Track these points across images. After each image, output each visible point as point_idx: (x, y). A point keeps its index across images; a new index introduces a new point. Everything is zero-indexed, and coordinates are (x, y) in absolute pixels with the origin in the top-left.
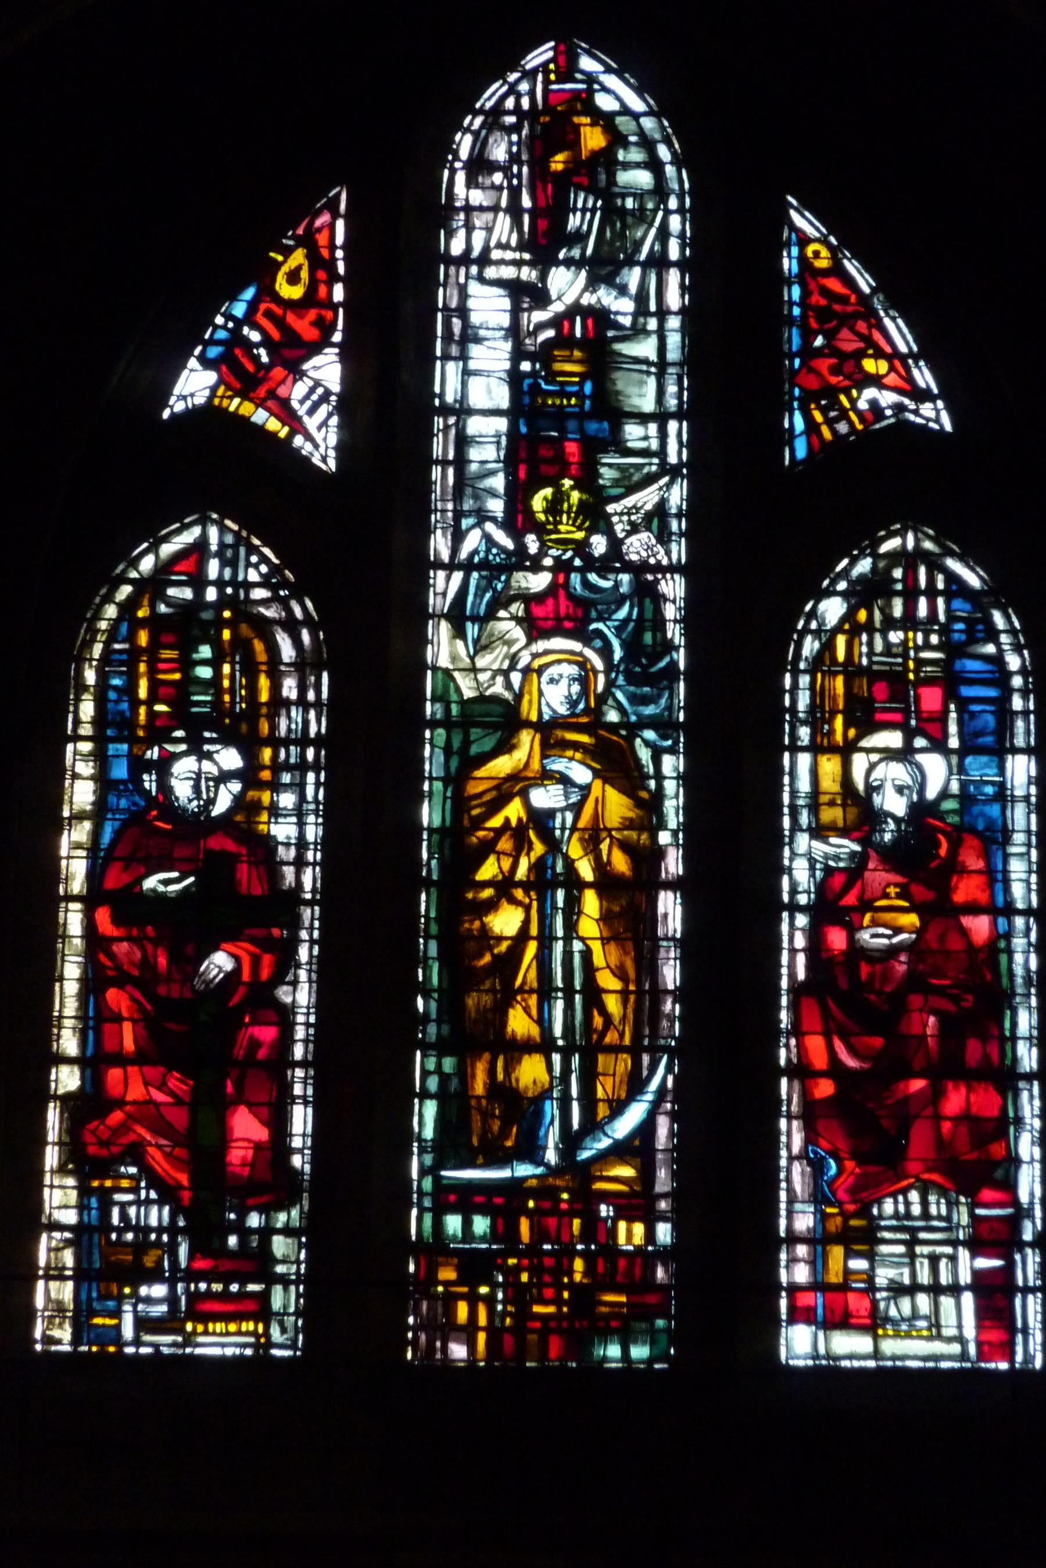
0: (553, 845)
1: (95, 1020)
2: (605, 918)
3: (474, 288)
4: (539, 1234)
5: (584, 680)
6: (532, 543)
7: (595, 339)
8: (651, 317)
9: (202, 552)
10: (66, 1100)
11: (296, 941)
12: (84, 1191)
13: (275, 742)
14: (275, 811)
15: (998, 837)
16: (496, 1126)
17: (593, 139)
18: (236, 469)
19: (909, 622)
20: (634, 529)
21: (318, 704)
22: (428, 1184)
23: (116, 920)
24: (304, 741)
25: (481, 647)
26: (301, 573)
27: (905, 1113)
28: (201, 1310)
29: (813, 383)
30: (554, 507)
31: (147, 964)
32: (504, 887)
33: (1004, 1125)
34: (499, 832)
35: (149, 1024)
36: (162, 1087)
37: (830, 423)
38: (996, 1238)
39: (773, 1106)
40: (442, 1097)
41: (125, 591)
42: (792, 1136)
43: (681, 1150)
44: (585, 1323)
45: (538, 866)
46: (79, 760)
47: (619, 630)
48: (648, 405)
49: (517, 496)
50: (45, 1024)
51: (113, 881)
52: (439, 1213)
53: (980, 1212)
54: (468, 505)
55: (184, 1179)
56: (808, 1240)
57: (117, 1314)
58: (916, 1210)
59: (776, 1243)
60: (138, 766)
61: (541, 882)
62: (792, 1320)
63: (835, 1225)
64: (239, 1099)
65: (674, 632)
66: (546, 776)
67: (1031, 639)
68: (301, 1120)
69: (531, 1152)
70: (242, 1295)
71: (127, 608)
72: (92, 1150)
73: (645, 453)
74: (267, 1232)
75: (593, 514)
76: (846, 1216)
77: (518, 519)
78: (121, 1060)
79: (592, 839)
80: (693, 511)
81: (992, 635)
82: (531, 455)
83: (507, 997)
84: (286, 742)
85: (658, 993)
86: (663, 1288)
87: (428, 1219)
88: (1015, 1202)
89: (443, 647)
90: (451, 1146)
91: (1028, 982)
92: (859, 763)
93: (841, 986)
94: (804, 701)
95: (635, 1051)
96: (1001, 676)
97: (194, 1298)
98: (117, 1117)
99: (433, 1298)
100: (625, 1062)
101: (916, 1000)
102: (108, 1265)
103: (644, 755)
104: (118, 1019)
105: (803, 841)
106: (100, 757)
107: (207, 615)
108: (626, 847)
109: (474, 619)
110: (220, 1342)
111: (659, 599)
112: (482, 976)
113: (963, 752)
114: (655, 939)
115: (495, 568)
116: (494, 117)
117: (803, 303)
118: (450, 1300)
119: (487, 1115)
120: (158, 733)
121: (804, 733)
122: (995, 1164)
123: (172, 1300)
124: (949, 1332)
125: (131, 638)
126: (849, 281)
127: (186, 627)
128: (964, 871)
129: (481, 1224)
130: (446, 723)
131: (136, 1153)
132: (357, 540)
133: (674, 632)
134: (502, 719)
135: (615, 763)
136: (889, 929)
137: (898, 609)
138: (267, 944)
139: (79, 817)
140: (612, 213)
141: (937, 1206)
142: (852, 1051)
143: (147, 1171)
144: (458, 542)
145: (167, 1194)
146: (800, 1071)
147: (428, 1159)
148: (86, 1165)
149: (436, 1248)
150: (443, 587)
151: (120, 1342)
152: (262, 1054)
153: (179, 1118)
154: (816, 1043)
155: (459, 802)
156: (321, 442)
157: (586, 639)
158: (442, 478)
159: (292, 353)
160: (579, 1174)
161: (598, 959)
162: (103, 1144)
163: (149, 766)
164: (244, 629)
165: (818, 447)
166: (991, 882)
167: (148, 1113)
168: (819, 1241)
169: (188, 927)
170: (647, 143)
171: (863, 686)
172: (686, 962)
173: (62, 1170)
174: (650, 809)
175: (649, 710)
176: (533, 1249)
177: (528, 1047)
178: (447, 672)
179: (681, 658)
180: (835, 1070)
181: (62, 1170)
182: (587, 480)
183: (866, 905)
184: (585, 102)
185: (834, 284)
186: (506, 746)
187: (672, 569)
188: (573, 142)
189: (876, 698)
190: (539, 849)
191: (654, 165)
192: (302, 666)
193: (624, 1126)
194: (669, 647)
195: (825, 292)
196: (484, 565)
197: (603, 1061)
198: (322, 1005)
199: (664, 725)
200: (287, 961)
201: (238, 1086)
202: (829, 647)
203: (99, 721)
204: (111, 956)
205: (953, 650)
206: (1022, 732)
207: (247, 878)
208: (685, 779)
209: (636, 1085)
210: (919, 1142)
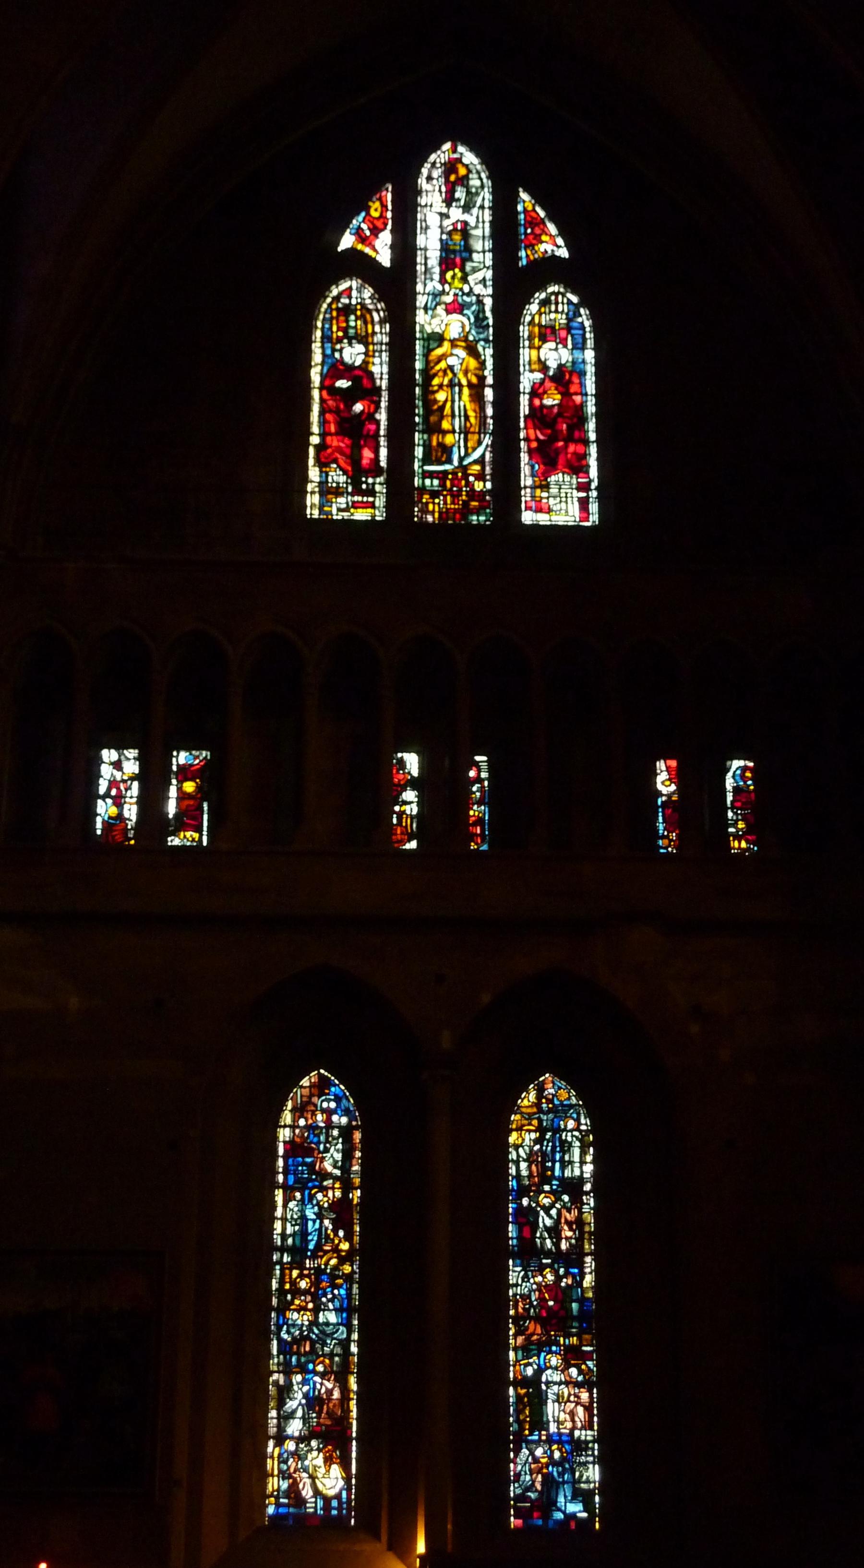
0: (455, 375)
1: (323, 423)
2: (470, 395)
3: (429, 214)
4: (452, 486)
5: (463, 327)
6: (447, 287)
7: (465, 231)
8: (481, 222)
9: (355, 291)
10: (316, 446)
11: (380, 401)
12: (321, 472)
13: (373, 344)
14: (373, 364)
15: (582, 374)
16: (439, 454)
17: (462, 171)
18: (359, 265)
19: (556, 311)
20: (476, 284)
21: (386, 333)
22: (420, 471)
23: (329, 394)
24: (381, 344)
25: (433, 317)
26: (381, 294)
27: (558, 451)
28: (356, 505)
29: (528, 243)
30: (453, 277)
31: (338, 407)
32: (441, 386)
33: (585, 456)
34: (439, 371)
35: (340, 424)
36: (343, 442)
37: (533, 254)
38: (584, 487)
39: (519, 450)
40: (424, 446)
41: (329, 300)
42: (524, 457)
43: (494, 462)
44: (466, 510)
45: (451, 381)
46: (316, 348)
47: (473, 313)
48: (480, 248)
49: (443, 274)
50: (308, 424)
51: (327, 383)
52: (424, 478)
53: (580, 480)
54: (428, 276)
55: (350, 469)
56: (531, 488)
57: (331, 506)
58: (561, 479)
59: (521, 489)
60: (334, 350)
61: (451, 385)
62: (526, 510)
63: (538, 483)
64: (365, 446)
65: (489, 314)
66: (452, 355)
67: (593, 316)
68: (383, 452)
69: (449, 461)
70: (367, 502)
71: (330, 305)
72: (323, 460)
73: (480, 262)
74: (374, 484)
75: (464, 279)
76: (541, 481)
77: (443, 281)
78: (331, 434)
79: (466, 372)
80: (494, 279)
81: (580, 316)
82: (446, 263)
83: (442, 417)
84: (376, 344)
85: (485, 417)
86: (489, 501)
87: (421, 481)
88: (589, 477)
89: (421, 317)
90: (426, 460)
91: (592, 415)
92: (543, 351)
93: (538, 415)
94: (526, 334)
95: (479, 433)
96: (583, 327)
97: (354, 502)
98: (329, 451)
99: (422, 503)
100: (476, 437)
101: (560, 420)
102: (327, 491)
103: (480, 349)
104: (329, 422)
105: (527, 374)
106: (323, 347)
107: (353, 307)
108: (476, 375)
109: (431, 309)
110: (361, 515)
111: (484, 305)
112: (434, 412)
113: (572, 349)
114: (484, 402)
115: (436, 295)
116: (434, 164)
117: (525, 219)
118: (427, 503)
119: (437, 451)
120: (340, 340)
121: (527, 343)
122: (583, 467)
123: (347, 503)
124: (571, 513)
125: (331, 313)
126: (537, 214)
127: (347, 310)
128: (573, 383)
129: (436, 482)
130: (423, 339)
131: (335, 461)
132: (396, 286)
133: (489, 314)
134: (439, 338)
135: (471, 350)
136: (552, 400)
137: (553, 308)
138: (373, 402)
139: (316, 365)
140: (468, 193)
141: (567, 478)
142: (542, 434)
143: (339, 466)
144: (425, 288)
145: (345, 472)
146: (527, 439)
147: (420, 464)
148: (322, 464)
149: (423, 490)
150: (421, 301)
151: (332, 515)
152: (371, 433)
153: (348, 451)
154: (531, 432)
155: (427, 362)
156: (385, 258)
157: (464, 315)
158: (420, 268)
159: (376, 231)
160: (464, 469)
161: (468, 407)
162: (326, 458)
163: (337, 350)
164: (364, 311)
165: (529, 261)
166: (581, 386)
167: (339, 449)
168: (533, 488)
169: (349, 396)
170: (478, 173)
171: (543, 330)
172: (494, 407)
173: (314, 466)
174: (482, 364)
175: (482, 336)
176: (451, 490)
177: (448, 432)
178: (423, 325)
179: (491, 322)
180: (537, 439)
181: (314, 466)
182: (463, 269)
183: (545, 392)
184: (459, 160)
185: (533, 214)
186: (440, 345)
187: (488, 296)
188: (456, 171)
189: (547, 333)
190: (450, 375)
191: (480, 179)
192: (382, 322)
193: (476, 455)
194: (487, 318)
195: (531, 216)
196: (433, 294)
197: (470, 436)
198: (389, 419)
199: (486, 340)
200: (378, 407)
201: (365, 441)
202: (533, 319)
203: (323, 337)
204: (327, 404)
205: (569, 320)
206: (590, 343)
207: (365, 382)
208: (493, 356)
209: (480, 443)
210: (561, 460)
